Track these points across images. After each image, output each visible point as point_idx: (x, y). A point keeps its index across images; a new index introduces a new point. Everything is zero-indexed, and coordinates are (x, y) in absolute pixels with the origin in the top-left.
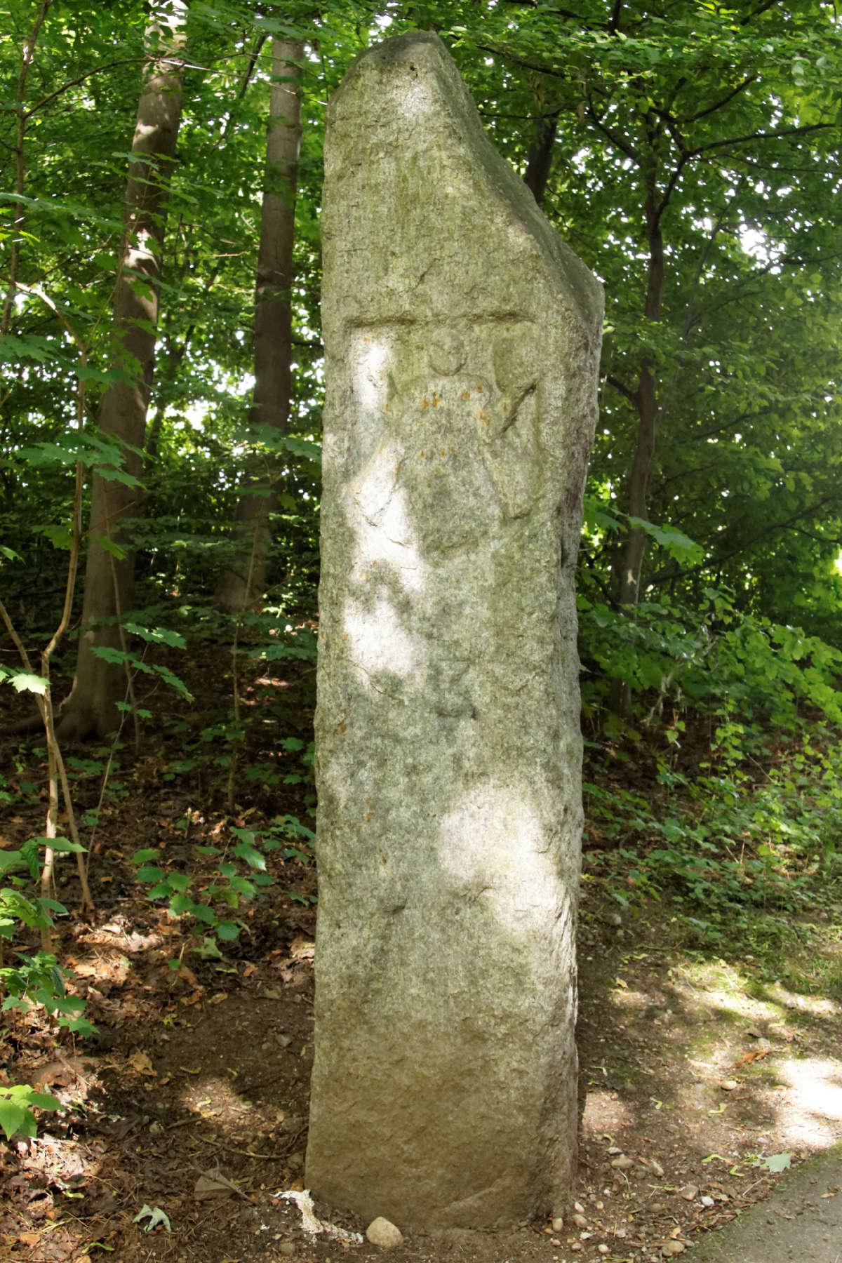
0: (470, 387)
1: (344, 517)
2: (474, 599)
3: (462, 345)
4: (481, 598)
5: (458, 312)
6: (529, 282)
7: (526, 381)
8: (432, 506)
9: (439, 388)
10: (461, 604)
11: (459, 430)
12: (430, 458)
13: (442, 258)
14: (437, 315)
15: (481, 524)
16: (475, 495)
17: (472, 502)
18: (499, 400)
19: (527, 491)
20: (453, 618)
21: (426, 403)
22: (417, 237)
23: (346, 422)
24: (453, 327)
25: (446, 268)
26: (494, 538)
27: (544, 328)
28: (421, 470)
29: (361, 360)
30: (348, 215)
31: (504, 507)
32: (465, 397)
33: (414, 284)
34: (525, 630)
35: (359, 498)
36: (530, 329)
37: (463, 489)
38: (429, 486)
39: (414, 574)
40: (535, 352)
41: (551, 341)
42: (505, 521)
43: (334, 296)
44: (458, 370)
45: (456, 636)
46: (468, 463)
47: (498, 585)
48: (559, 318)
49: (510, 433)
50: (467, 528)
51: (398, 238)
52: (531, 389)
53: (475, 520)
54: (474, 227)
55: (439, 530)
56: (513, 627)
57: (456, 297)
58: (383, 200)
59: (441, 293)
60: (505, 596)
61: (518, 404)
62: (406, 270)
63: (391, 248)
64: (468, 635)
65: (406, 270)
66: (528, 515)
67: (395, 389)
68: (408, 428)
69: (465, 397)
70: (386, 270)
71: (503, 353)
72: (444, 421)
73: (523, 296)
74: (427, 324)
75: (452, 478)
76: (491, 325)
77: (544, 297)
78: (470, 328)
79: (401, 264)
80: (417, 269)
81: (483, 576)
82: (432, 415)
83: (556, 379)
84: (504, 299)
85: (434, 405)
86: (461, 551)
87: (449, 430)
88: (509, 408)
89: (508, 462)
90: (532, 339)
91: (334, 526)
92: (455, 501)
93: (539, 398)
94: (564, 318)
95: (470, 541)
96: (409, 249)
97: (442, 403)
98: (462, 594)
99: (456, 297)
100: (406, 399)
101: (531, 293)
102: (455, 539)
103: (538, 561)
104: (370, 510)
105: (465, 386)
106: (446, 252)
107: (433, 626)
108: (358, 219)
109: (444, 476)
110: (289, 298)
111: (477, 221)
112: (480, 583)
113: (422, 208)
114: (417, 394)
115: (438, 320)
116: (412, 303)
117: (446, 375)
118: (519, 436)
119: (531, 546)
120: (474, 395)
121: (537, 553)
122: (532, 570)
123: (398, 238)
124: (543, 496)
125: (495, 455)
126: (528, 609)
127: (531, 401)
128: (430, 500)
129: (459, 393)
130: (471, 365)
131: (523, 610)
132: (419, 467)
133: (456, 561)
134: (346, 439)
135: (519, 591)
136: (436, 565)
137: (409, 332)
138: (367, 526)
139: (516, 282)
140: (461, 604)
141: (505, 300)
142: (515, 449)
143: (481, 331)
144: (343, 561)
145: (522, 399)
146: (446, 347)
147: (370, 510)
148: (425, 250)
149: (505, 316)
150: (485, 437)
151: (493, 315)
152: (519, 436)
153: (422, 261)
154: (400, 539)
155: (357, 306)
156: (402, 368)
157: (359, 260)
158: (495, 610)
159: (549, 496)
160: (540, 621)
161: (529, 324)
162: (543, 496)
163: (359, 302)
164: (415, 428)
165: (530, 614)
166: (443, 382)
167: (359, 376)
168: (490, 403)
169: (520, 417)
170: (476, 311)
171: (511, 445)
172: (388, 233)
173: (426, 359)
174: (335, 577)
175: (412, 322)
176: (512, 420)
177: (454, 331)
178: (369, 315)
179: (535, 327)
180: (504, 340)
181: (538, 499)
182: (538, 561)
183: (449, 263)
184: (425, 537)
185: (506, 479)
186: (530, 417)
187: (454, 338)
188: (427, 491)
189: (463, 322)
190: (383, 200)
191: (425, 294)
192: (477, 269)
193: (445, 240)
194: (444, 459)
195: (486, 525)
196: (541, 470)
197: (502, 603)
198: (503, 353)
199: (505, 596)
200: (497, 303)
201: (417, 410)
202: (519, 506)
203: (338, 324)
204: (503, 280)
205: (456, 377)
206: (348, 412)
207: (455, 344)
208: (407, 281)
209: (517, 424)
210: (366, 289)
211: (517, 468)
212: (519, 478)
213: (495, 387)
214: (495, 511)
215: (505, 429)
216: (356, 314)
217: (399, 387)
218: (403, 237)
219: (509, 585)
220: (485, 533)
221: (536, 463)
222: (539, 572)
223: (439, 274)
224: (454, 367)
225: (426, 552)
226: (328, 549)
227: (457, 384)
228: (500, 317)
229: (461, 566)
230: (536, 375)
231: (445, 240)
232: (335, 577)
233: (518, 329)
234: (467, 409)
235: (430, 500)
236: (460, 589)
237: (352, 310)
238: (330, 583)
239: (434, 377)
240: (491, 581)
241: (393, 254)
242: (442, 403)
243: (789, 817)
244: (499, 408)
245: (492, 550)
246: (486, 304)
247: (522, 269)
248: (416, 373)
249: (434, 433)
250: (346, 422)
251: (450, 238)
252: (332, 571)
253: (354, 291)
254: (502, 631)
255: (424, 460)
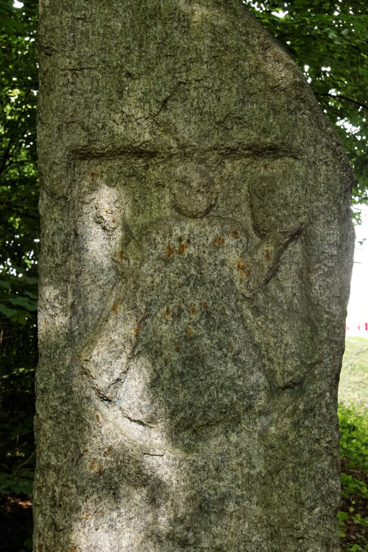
0: (223, 232)
1: (70, 392)
2: (239, 492)
3: (211, 182)
4: (248, 490)
5: (208, 144)
6: (291, 112)
7: (292, 225)
8: (181, 375)
9: (186, 232)
10: (223, 499)
11: (212, 282)
12: (178, 316)
13: (187, 82)
14: (183, 147)
15: (244, 396)
16: (235, 360)
17: (231, 369)
18: (258, 247)
19: (299, 355)
20: (213, 517)
21: (170, 250)
22: (159, 57)
23: (69, 272)
24: (202, 161)
25: (194, 94)
26: (260, 413)
27: (312, 164)
28: (166, 330)
29: (87, 198)
30: (72, 29)
31: (270, 375)
32: (218, 243)
33: (155, 110)
34: (306, 531)
35: (90, 367)
36: (292, 166)
37: (219, 354)
38: (178, 350)
39: (164, 461)
40: (301, 193)
41: (321, 179)
42: (274, 391)
43: (55, 122)
44: (207, 211)
45: (218, 542)
46: (225, 322)
47: (270, 473)
48: (329, 154)
49: (272, 286)
50: (226, 401)
51: (134, 57)
52: (295, 235)
53: (236, 391)
54: (227, 47)
55: (191, 405)
56: (291, 527)
57: (206, 127)
58: (116, 13)
59: (188, 122)
60: (279, 486)
61: (281, 252)
62: (145, 94)
63: (127, 68)
64: (235, 540)
65: (145, 94)
66: (300, 383)
67: (134, 236)
68: (149, 279)
69: (218, 243)
70: (120, 93)
71: (261, 194)
72: (193, 272)
73: (286, 128)
74: (171, 156)
75: (206, 341)
76: (245, 161)
77: (310, 130)
78: (221, 164)
79: (139, 86)
80: (159, 93)
81: (249, 462)
82: (177, 264)
83: (328, 222)
84: (264, 131)
85: (181, 252)
86: (219, 429)
87: (200, 281)
88: (272, 256)
89: (273, 321)
90: (298, 177)
91: (55, 403)
92: (210, 368)
93: (307, 244)
94: (335, 154)
95: (230, 418)
96: (150, 69)
97: (191, 250)
98: (223, 486)
99: (206, 127)
100: (145, 245)
101: (295, 126)
102: (211, 415)
103: (318, 441)
104: (103, 381)
105: (217, 231)
106: (193, 76)
107: (188, 529)
108: (85, 34)
109: (196, 337)
110: (16, 110)
111: (232, 42)
112: (246, 470)
113: (164, 24)
114: (159, 239)
115: (185, 153)
116: (152, 133)
117: (194, 217)
118: (282, 289)
119: (307, 423)
120: (229, 240)
121: (315, 431)
122: (311, 452)
123: (134, 57)
124: (320, 362)
125: (257, 311)
126: (309, 503)
127: (297, 247)
128: (179, 368)
129: (211, 239)
130: (222, 207)
131: (302, 504)
132: (165, 327)
133: (213, 443)
134: (70, 293)
135: (296, 479)
136: (188, 449)
137: (147, 167)
138: (97, 402)
139: (276, 112)
140: (223, 499)
141: (265, 132)
142: (280, 305)
143: (234, 168)
144: (68, 448)
145: (286, 246)
146: (194, 184)
147: (103, 381)
148: (169, 72)
149: (264, 150)
150: (244, 291)
151: (249, 149)
152: (282, 289)
153: (164, 84)
154: (140, 417)
155: (84, 134)
156: (137, 211)
157: (87, 80)
158: (268, 506)
159: (326, 360)
160: (323, 517)
161: (292, 160)
162: (320, 362)
163: (87, 129)
164: (158, 280)
165: (312, 509)
166: (190, 226)
167: (85, 217)
168: (248, 251)
169: (283, 268)
170: (229, 144)
171: (274, 299)
172: (122, 50)
173: (168, 199)
174: (57, 470)
175: (152, 155)
176: (274, 270)
177: (202, 167)
178: (98, 145)
179: (298, 164)
180: (263, 178)
181: (312, 365)
182: (318, 441)
183: (196, 89)
184: (173, 414)
185: (272, 340)
186: (294, 267)
187: (203, 174)
188: (175, 357)
189: (213, 157)
190: (116, 13)
191: (168, 122)
192: (230, 97)
193: (192, 61)
194: (195, 317)
195: (250, 397)
196: (314, 330)
197: (276, 497)
198: (261, 194)
199: (279, 486)
200: (255, 135)
201: (159, 258)
202: (290, 374)
203: (60, 154)
204: (262, 110)
205: (205, 220)
206: (71, 261)
207: (205, 181)
208: (147, 106)
209: (279, 275)
210: (95, 114)
211: (285, 327)
212: (289, 339)
213: (252, 232)
214: (258, 378)
215: (267, 281)
216: (83, 143)
217: (134, 230)
218: (140, 57)
219: (283, 473)
220: (250, 407)
221: (308, 321)
222: (319, 455)
223: (185, 99)
224: (203, 208)
225: (175, 435)
226: (46, 429)
227: (208, 228)
228: (257, 152)
229: (219, 450)
230: (303, 218)
231: (192, 61)
232: (57, 470)
233: (277, 166)
234: (221, 257)
235: (179, 368)
236: (221, 479)
237: (79, 139)
238: (51, 478)
239: (178, 220)
240: (260, 467)
241: (129, 75)
242: (191, 250)
243: (100, 471)
244: (259, 256)
245: (259, 428)
246: (240, 136)
247: (284, 99)
248: (156, 215)
249: (181, 286)
250: (69, 272)
251: (199, 59)
252: (53, 461)
253: (80, 116)
254: (277, 532)
255: (170, 318)
